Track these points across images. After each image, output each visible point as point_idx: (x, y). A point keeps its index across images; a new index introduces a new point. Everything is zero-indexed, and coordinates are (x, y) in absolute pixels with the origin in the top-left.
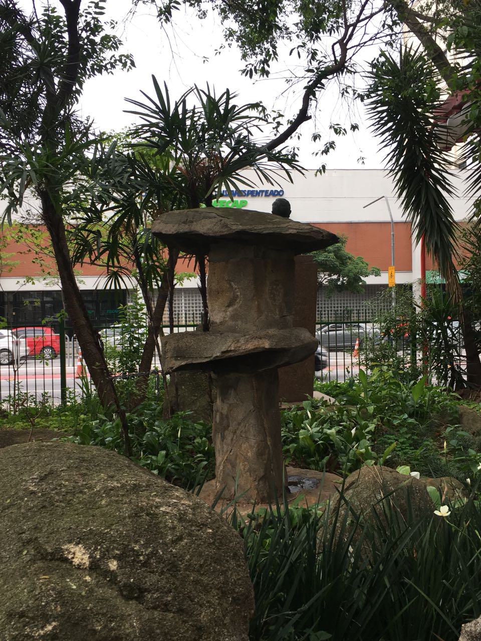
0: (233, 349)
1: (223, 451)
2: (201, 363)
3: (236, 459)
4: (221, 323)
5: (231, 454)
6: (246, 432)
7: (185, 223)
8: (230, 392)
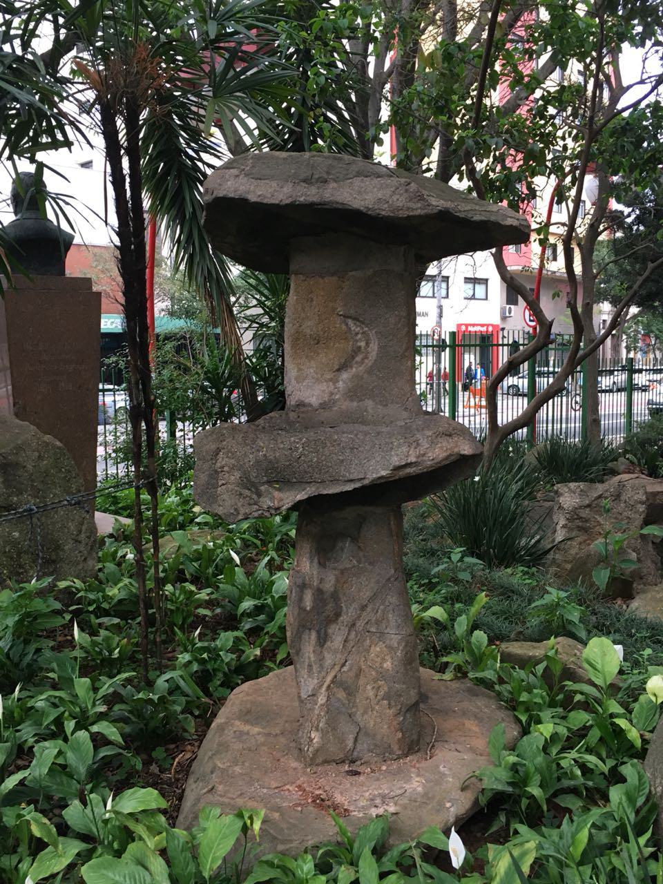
0: (414, 460)
1: (321, 666)
2: (342, 494)
3: (358, 676)
4: (324, 406)
5: (345, 669)
6: (378, 623)
7: (307, 181)
8: (340, 544)
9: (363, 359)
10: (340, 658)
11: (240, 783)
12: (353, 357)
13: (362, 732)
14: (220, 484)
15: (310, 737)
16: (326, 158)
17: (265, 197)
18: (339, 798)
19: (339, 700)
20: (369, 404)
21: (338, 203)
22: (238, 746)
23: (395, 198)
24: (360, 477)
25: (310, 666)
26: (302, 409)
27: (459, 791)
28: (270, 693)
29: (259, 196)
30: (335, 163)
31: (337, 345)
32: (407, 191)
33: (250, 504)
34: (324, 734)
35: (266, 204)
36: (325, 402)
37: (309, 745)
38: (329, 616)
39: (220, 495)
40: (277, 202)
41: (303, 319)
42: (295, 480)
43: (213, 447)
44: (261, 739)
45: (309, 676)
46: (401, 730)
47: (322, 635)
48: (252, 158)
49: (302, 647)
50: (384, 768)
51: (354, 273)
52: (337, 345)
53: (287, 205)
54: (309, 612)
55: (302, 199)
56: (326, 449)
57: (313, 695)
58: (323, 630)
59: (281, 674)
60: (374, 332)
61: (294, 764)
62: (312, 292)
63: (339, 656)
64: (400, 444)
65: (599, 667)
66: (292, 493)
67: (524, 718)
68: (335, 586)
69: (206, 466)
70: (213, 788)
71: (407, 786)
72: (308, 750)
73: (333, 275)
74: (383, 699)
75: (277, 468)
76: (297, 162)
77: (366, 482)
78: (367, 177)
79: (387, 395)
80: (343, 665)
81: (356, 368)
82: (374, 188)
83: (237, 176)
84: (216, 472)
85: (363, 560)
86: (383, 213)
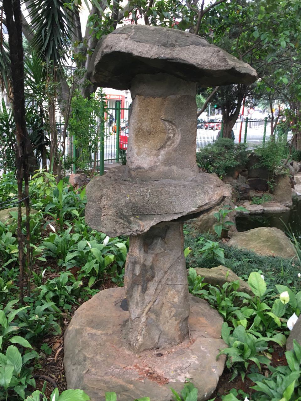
1: (143, 303)
3: (162, 307)
4: (151, 169)
5: (155, 304)
7: (165, 45)
8: (155, 241)
9: (171, 143)
10: (153, 298)
11: (103, 366)
12: (166, 142)
13: (162, 333)
14: (103, 215)
15: (137, 339)
16: (175, 32)
17: (143, 53)
18: (159, 371)
19: (152, 319)
20: (174, 168)
21: (180, 59)
22: (93, 343)
23: (213, 59)
24: (181, 211)
25: (137, 303)
26: (139, 170)
27: (216, 361)
28: (98, 309)
29: (140, 52)
30: (180, 35)
31: (160, 136)
32: (218, 55)
33: (124, 228)
34: (144, 337)
35: (143, 58)
36: (152, 166)
37: (137, 343)
38: (148, 278)
39: (103, 221)
40: (149, 57)
41: (143, 121)
42: (146, 213)
43: (99, 194)
44: (104, 338)
45: (136, 308)
46: (180, 330)
47: (144, 287)
48: (134, 28)
49: (133, 294)
50: (173, 350)
51: (171, 96)
52: (160, 136)
53: (155, 59)
54: (138, 276)
55: (162, 56)
56: (162, 196)
57: (139, 317)
58: (145, 285)
59: (99, 296)
60: (179, 129)
61: (128, 352)
62: (148, 106)
63: (152, 297)
64: (199, 193)
65: (257, 287)
66: (148, 222)
67: (225, 314)
68: (152, 262)
69: (94, 205)
70: (88, 370)
71: (190, 361)
72: (136, 345)
73: (160, 97)
74: (173, 317)
75: (137, 207)
76: (159, 33)
77: (184, 214)
78: (197, 45)
79: (183, 163)
80: (155, 302)
81: (168, 148)
82: (201, 52)
83: (126, 39)
84: (101, 208)
85: (167, 248)
86: (206, 67)
